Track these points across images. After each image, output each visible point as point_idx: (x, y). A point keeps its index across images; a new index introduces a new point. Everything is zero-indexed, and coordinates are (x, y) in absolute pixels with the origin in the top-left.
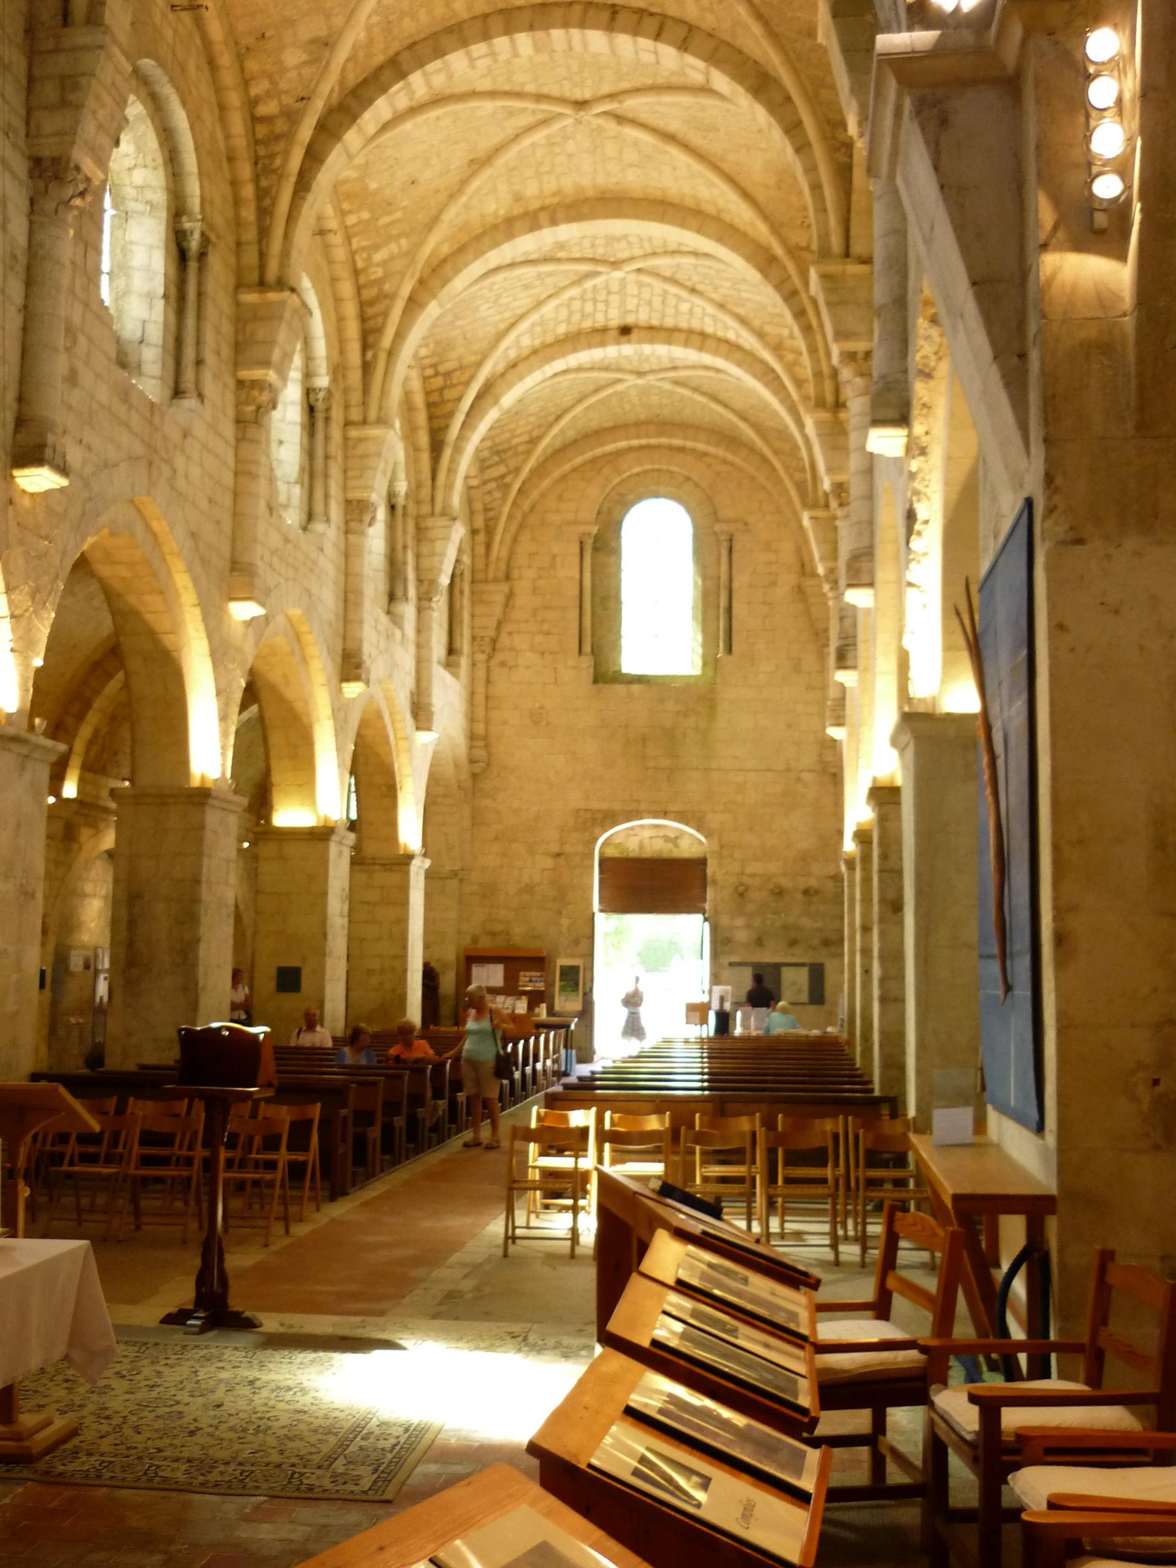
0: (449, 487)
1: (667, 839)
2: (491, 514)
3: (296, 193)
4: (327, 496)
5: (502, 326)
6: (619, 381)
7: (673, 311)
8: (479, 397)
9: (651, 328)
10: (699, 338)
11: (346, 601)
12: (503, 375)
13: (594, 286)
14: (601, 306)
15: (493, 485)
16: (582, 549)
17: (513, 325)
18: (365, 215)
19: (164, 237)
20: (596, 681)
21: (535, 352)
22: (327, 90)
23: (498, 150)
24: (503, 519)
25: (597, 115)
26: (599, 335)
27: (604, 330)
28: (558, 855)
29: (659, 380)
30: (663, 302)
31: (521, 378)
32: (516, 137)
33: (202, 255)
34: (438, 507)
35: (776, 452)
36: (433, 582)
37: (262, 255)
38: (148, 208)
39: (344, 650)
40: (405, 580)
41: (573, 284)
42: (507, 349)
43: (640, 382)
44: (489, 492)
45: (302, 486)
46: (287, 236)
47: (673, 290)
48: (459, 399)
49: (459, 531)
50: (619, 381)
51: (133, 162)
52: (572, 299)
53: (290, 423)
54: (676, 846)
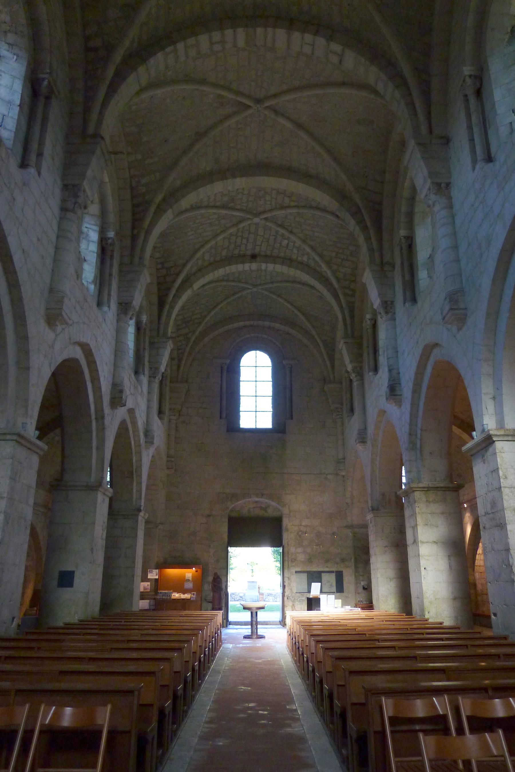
0: (167, 324)
1: (261, 508)
2: (180, 351)
3: (107, 93)
4: (109, 295)
5: (197, 247)
6: (245, 289)
7: (278, 245)
8: (184, 282)
9: (266, 256)
10: (289, 261)
11: (115, 356)
12: (194, 274)
13: (244, 227)
14: (244, 241)
15: (181, 338)
16: (222, 370)
17: (202, 246)
18: (139, 157)
19: (23, 75)
20: (228, 431)
21: (211, 264)
22: (133, 35)
23: (212, 128)
24: (186, 354)
25: (267, 108)
26: (241, 258)
27: (244, 256)
28: (209, 516)
29: (262, 289)
30: (275, 239)
31: (203, 276)
32: (221, 121)
33: (48, 98)
34: (161, 332)
35: (314, 327)
36: (157, 369)
37: (85, 121)
38: (15, 57)
39: (113, 382)
40: (144, 365)
41: (233, 225)
42: (198, 259)
43: (255, 290)
44: (180, 341)
45: (95, 285)
46: (101, 114)
47: (281, 231)
48: (174, 282)
49: (169, 346)
50: (245, 289)
51: (8, 28)
52: (231, 234)
53: (91, 251)
54: (266, 511)
